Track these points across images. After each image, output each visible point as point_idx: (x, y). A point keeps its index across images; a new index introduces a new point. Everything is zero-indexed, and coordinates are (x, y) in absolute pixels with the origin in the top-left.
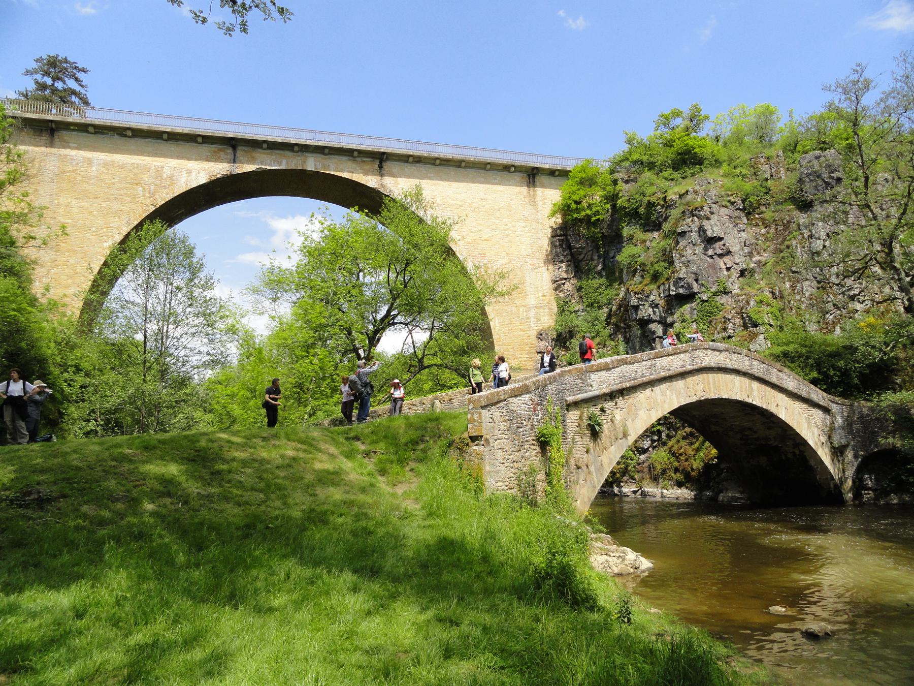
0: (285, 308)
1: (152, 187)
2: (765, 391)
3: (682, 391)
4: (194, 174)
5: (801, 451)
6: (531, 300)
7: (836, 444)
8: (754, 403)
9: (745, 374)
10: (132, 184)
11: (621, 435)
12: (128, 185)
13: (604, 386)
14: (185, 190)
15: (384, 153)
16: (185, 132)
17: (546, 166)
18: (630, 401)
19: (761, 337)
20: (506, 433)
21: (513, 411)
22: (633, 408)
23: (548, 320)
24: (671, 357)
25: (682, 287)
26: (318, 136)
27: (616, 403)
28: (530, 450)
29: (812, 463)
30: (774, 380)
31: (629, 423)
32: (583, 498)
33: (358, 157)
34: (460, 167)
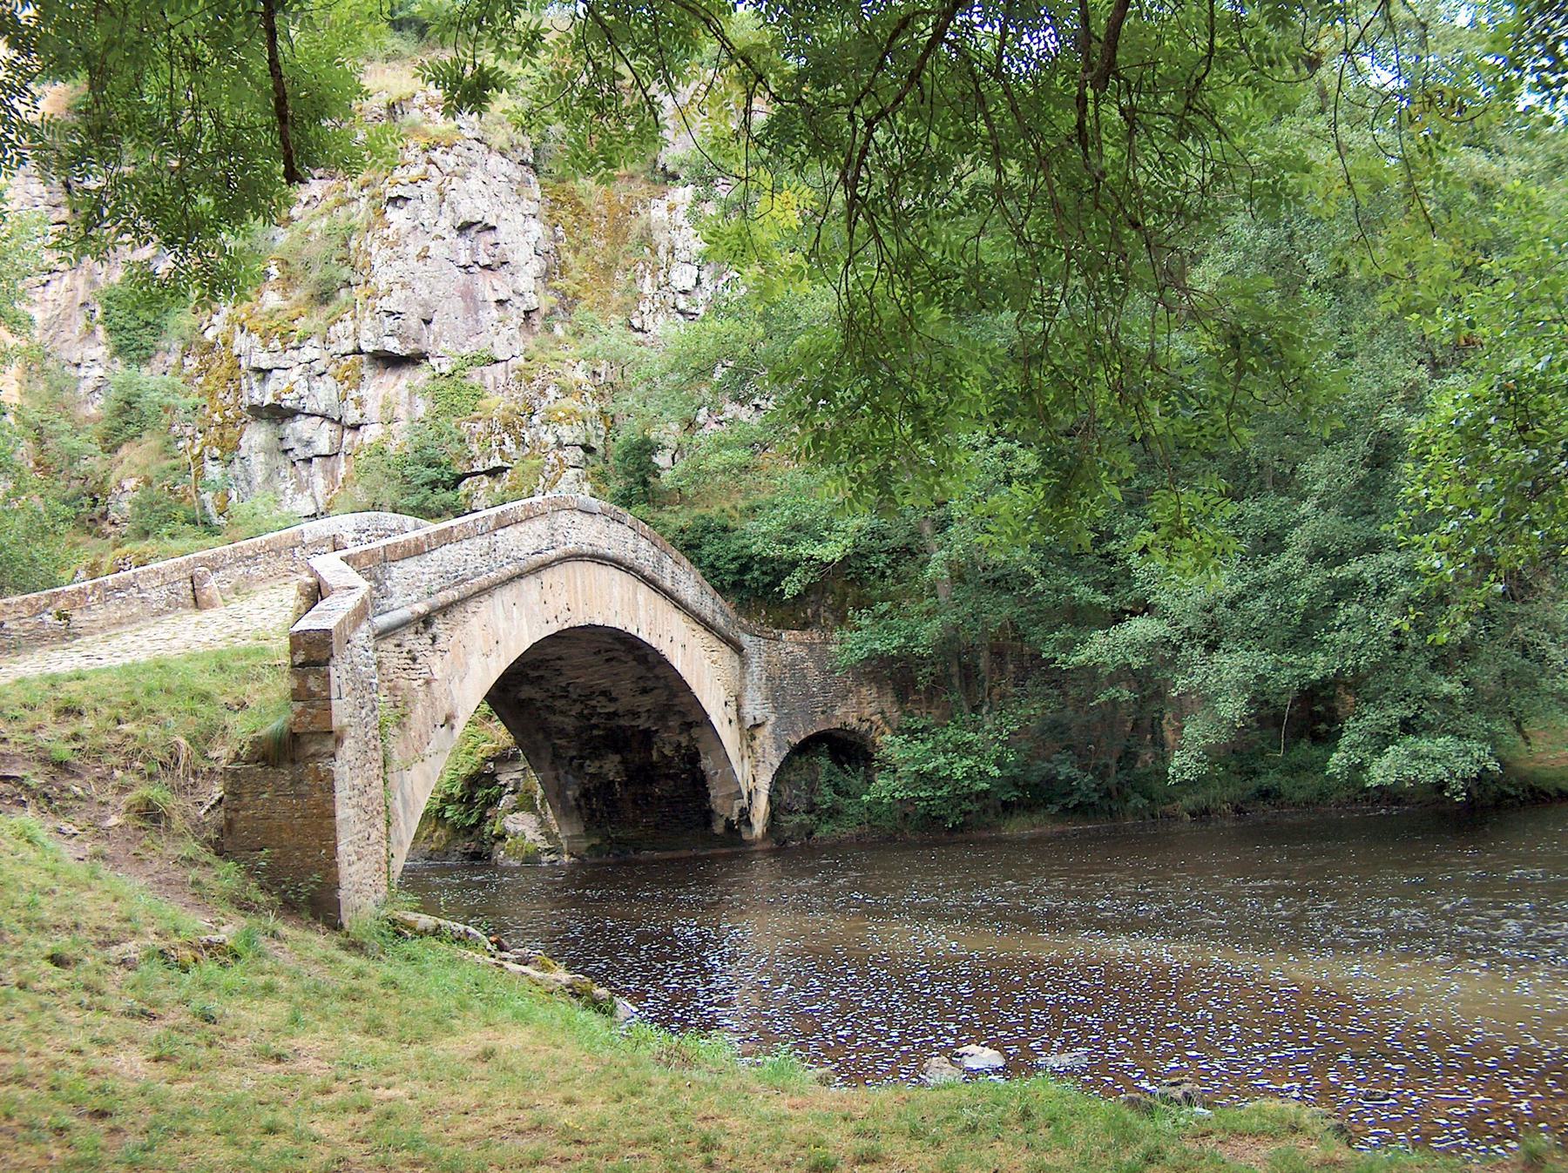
27: (434, 639)
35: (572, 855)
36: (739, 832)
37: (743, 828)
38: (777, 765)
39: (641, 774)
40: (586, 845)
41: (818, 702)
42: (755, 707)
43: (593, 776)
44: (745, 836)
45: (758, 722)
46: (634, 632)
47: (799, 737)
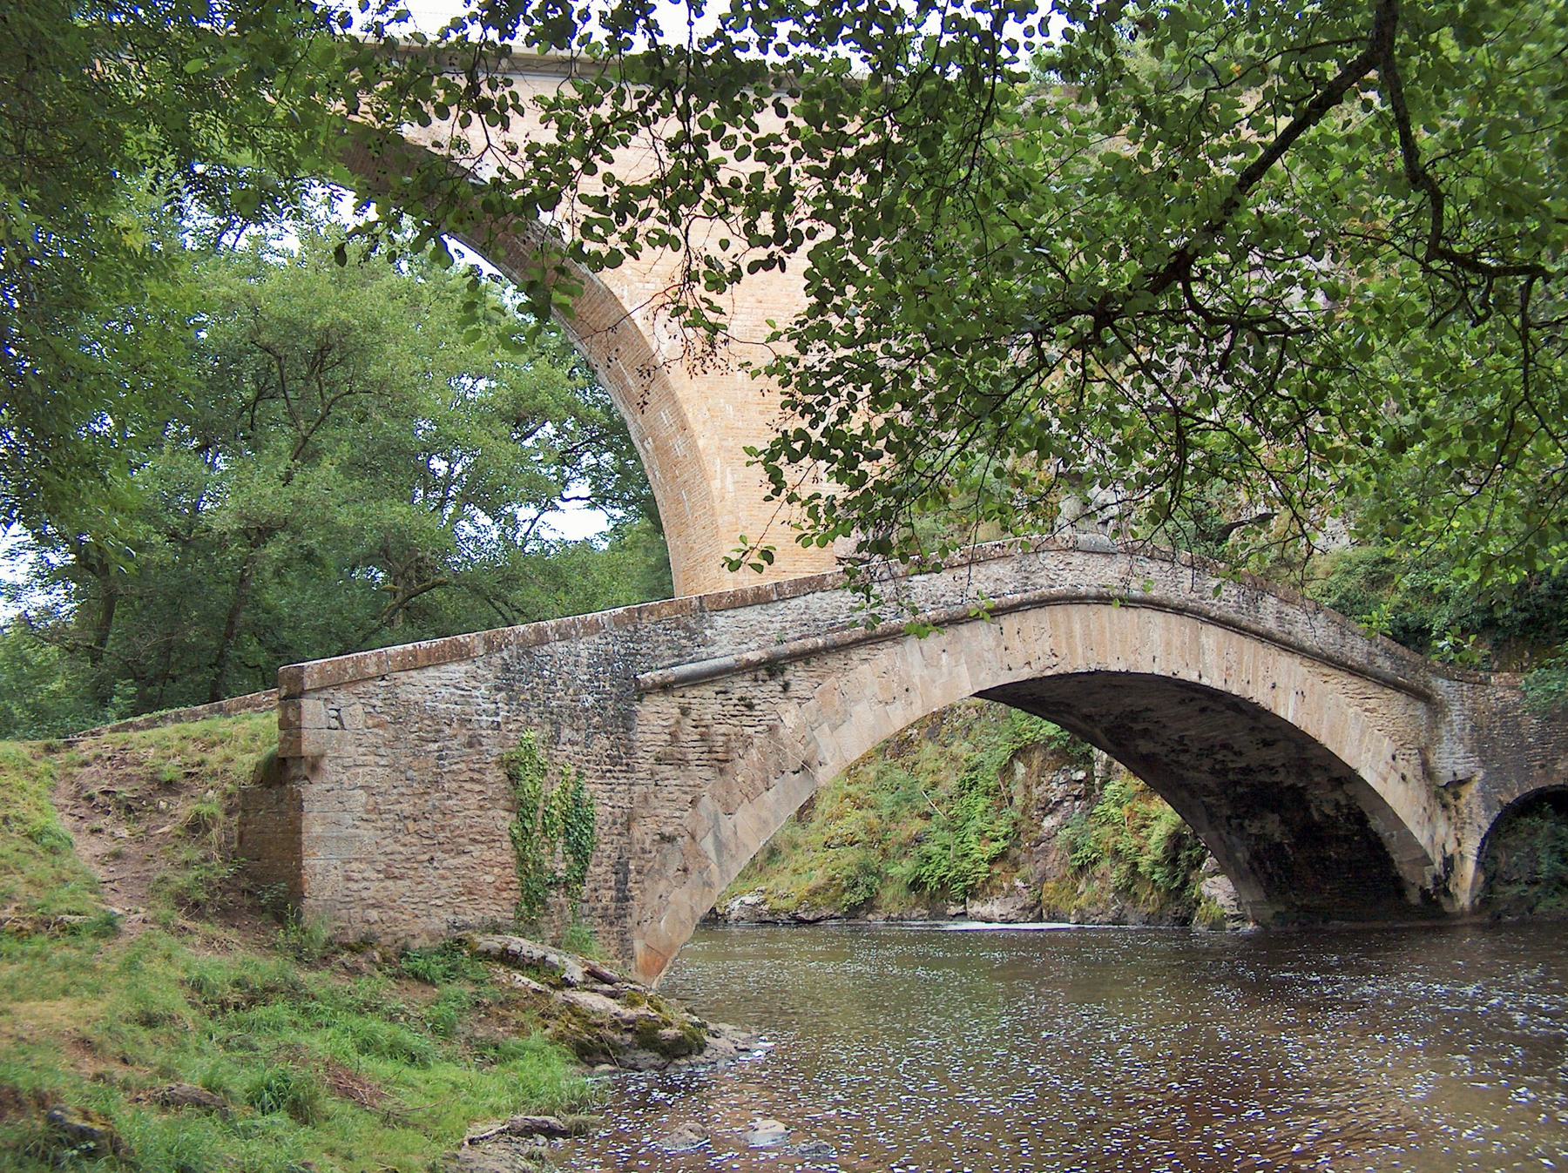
2: (1240, 654)
5: (1348, 797)
7: (1445, 776)
8: (1205, 681)
13: (753, 645)
20: (382, 751)
27: (786, 687)
28: (463, 795)
31: (824, 737)
35: (1257, 922)
36: (1437, 903)
37: (1443, 899)
38: (1486, 827)
39: (1311, 834)
40: (1271, 912)
41: (1536, 754)
42: (1452, 759)
43: (1258, 838)
44: (1447, 908)
45: (1460, 777)
46: (1194, 678)
47: (1512, 795)
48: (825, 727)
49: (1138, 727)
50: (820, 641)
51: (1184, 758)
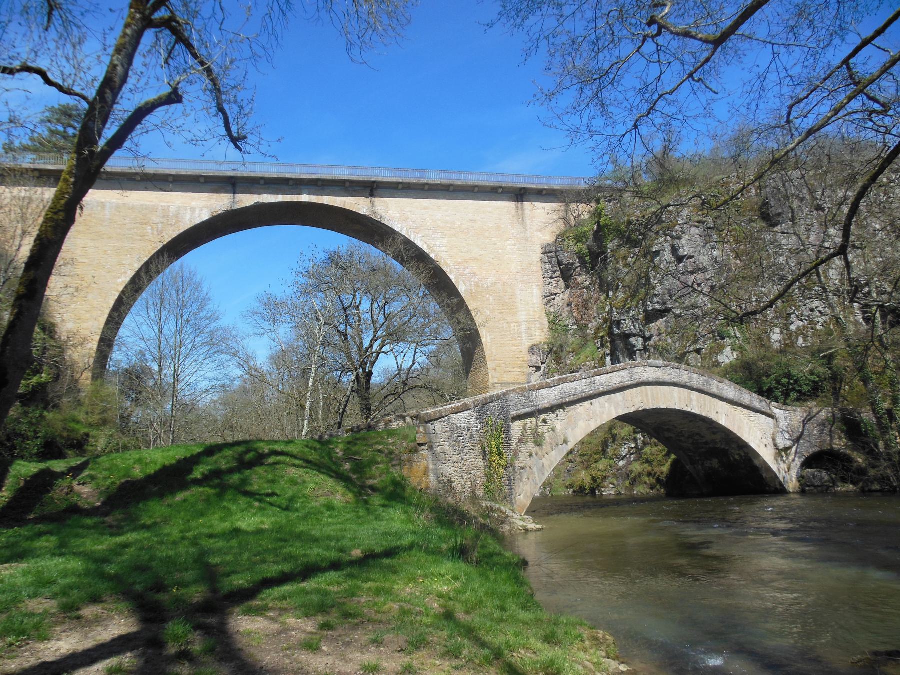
0: (285, 332)
1: (160, 226)
3: (621, 404)
4: (197, 212)
5: (745, 453)
6: (522, 316)
7: (781, 446)
8: (693, 411)
9: (684, 386)
10: (141, 224)
11: (561, 442)
12: (138, 225)
14: (189, 227)
15: (374, 182)
16: (189, 174)
17: (534, 186)
18: (570, 413)
19: (728, 349)
21: (453, 425)
22: (573, 419)
23: (540, 334)
24: (610, 375)
25: (658, 302)
26: (312, 170)
27: (557, 416)
29: (756, 462)
30: (714, 390)
32: (526, 493)
33: (350, 186)
34: (448, 190)
48: (570, 430)
49: (666, 428)
50: (567, 400)
51: (683, 439)
